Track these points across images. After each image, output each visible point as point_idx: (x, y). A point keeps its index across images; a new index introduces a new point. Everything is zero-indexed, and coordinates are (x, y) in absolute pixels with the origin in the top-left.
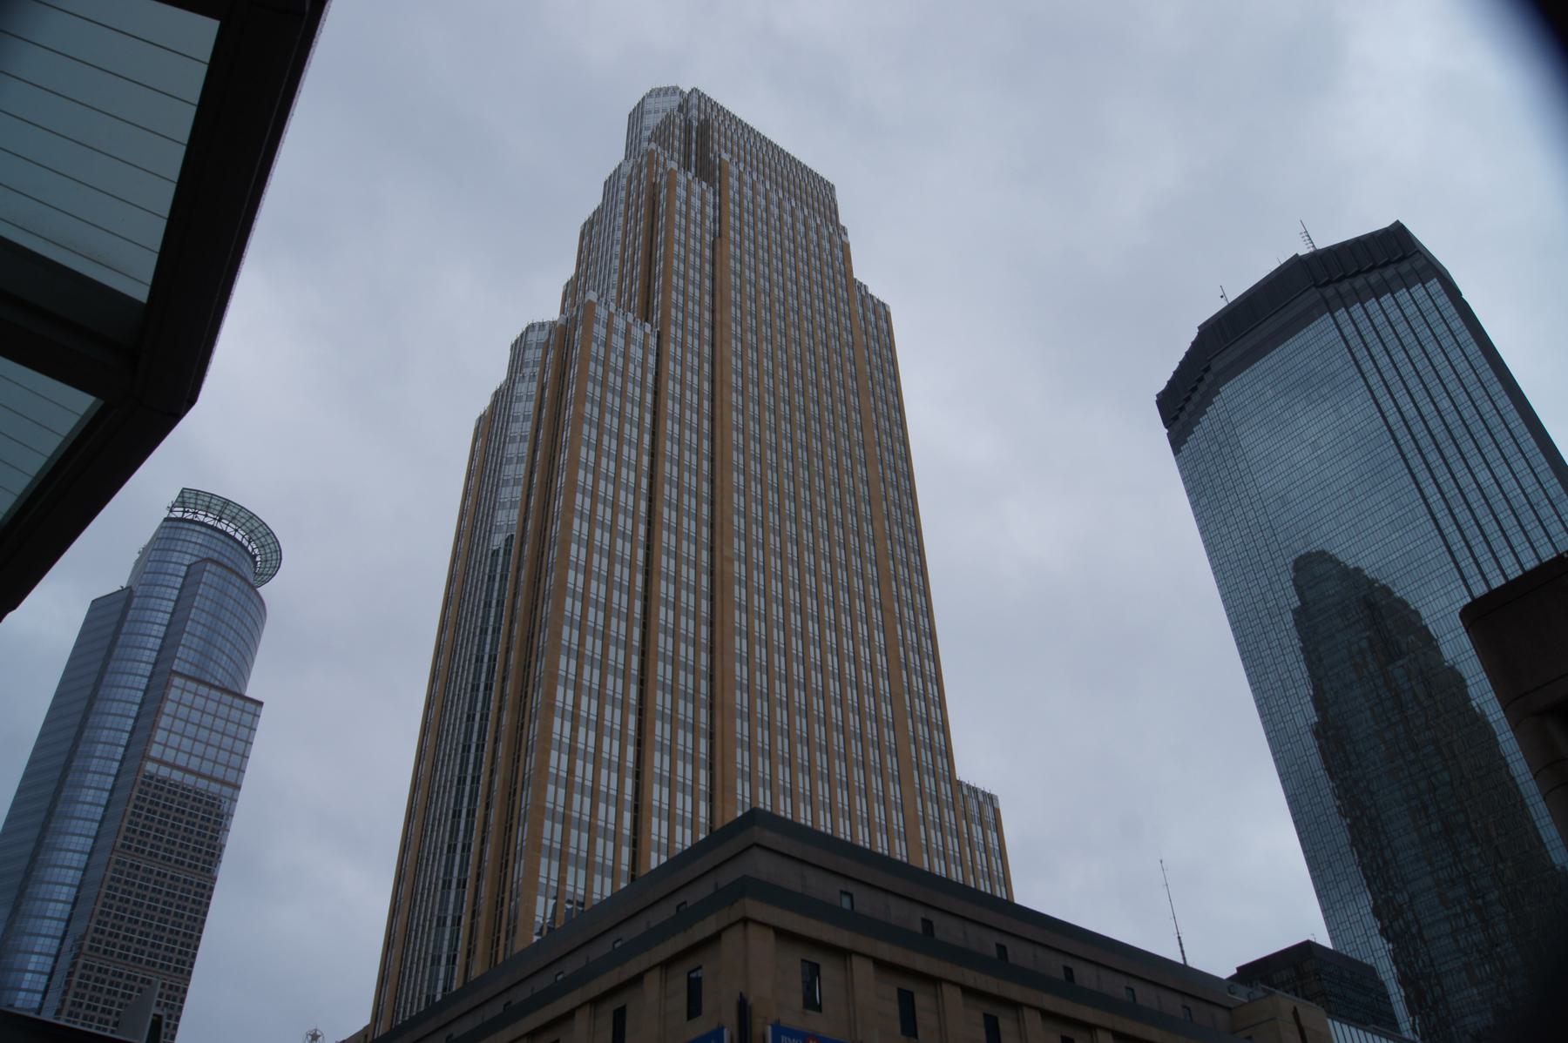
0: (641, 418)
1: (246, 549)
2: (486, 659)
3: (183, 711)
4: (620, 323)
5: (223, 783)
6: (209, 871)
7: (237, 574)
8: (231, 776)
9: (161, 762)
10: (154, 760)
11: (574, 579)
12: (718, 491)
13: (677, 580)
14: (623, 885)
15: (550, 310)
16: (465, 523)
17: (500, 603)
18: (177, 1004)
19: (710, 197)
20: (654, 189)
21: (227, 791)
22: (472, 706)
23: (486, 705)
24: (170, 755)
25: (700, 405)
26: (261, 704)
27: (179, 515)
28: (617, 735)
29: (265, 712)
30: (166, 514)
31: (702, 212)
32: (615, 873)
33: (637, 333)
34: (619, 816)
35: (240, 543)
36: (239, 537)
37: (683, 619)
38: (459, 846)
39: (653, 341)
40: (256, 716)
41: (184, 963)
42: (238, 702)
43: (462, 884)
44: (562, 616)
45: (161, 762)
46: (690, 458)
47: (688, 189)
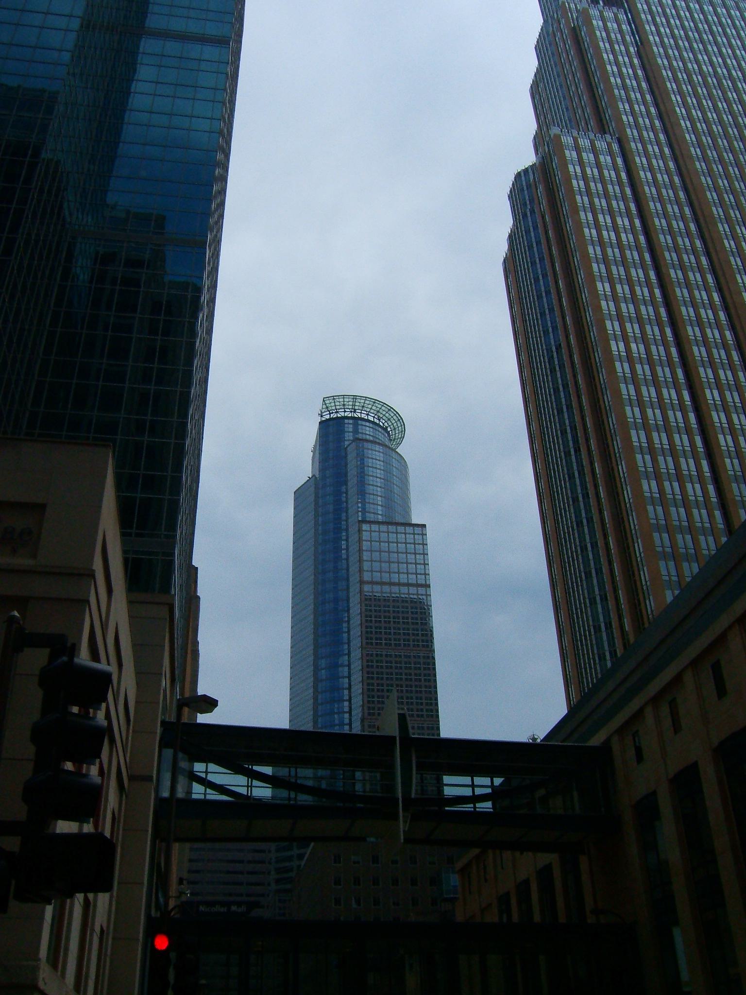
0: (627, 208)
1: (378, 425)
2: (569, 430)
3: (376, 555)
4: (584, 142)
5: (418, 585)
6: (427, 646)
7: (379, 444)
8: (421, 580)
9: (372, 583)
10: (368, 583)
11: (632, 413)
12: (654, 84)
13: (705, 342)
14: (724, 539)
15: (528, 158)
16: (537, 446)
17: (565, 386)
18: (433, 690)
19: (622, 16)
20: (575, 33)
21: (422, 591)
22: (582, 539)
23: (588, 510)
24: (377, 576)
25: (671, 181)
26: (424, 526)
27: (328, 417)
28: (689, 454)
29: (429, 531)
30: (319, 419)
31: (621, 31)
32: (713, 531)
33: (601, 145)
34: (710, 515)
35: (373, 423)
36: (371, 419)
37: (721, 372)
38: (593, 571)
39: (615, 147)
40: (424, 535)
41: (427, 641)
42: (409, 530)
43: (604, 598)
44: (617, 377)
45: (372, 583)
46: (684, 242)
47: (603, 19)
